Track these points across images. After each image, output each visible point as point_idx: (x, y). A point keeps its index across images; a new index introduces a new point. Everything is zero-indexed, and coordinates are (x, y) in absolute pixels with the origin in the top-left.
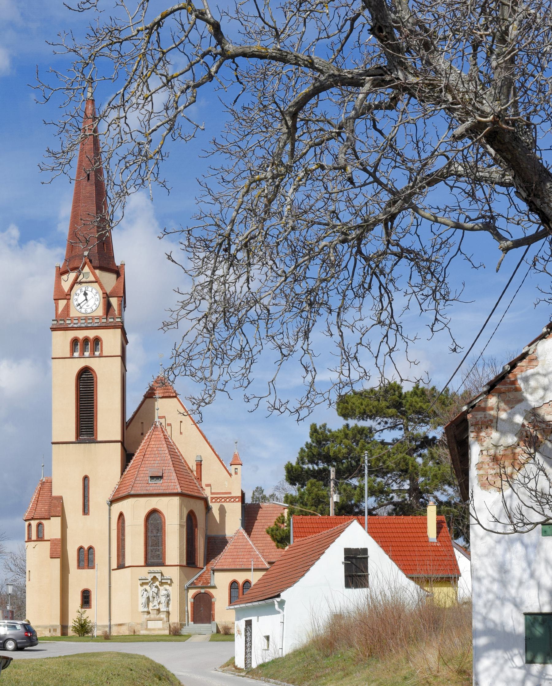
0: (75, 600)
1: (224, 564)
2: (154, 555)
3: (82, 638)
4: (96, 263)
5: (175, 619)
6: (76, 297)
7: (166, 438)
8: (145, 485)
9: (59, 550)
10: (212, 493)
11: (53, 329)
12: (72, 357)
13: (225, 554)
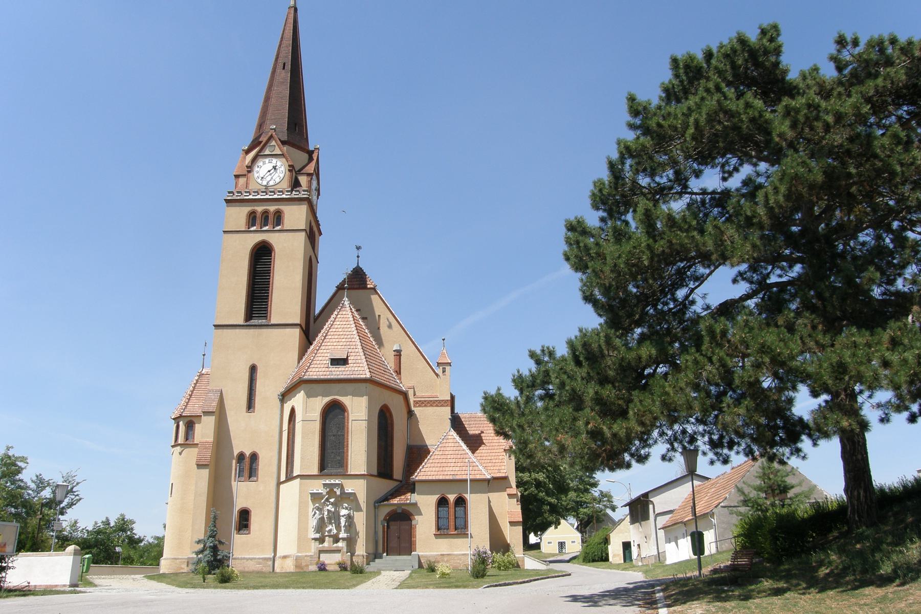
2: (331, 455)
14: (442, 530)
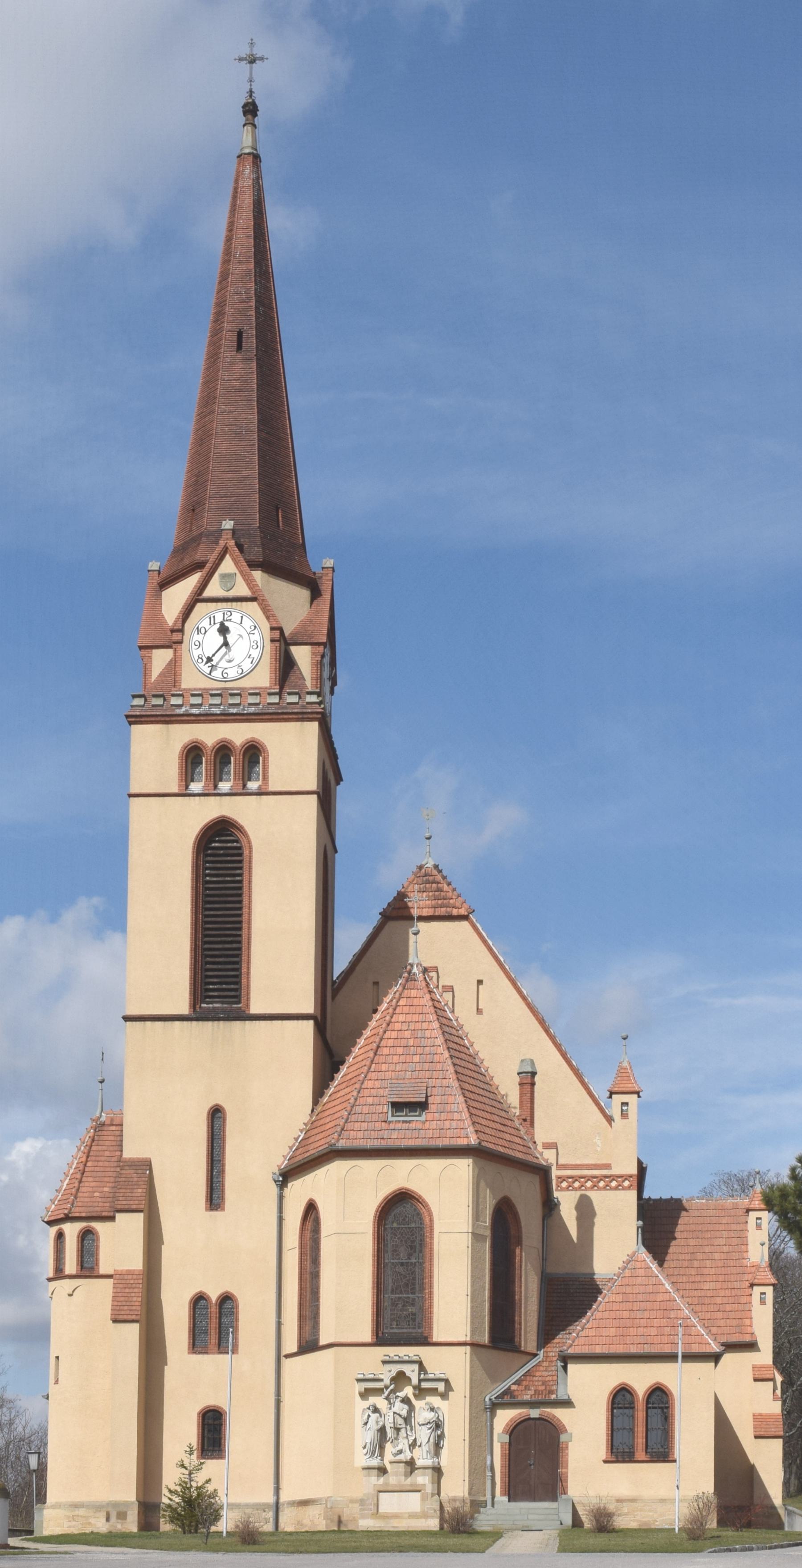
0: (180, 1433)
1: (596, 1340)
2: (400, 1314)
3: (189, 1539)
4: (256, 552)
5: (456, 1487)
6: (197, 637)
7: (438, 1009)
8: (378, 1125)
9: (140, 1303)
10: (560, 1167)
11: (134, 719)
12: (185, 794)
13: (598, 1315)
14: (620, 1452)
